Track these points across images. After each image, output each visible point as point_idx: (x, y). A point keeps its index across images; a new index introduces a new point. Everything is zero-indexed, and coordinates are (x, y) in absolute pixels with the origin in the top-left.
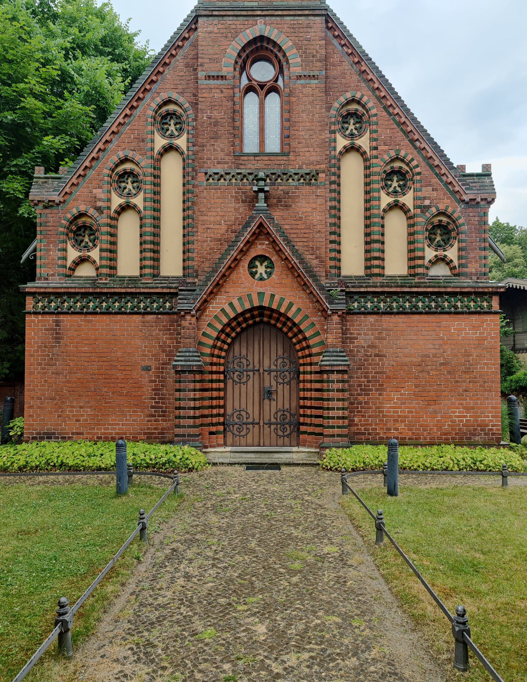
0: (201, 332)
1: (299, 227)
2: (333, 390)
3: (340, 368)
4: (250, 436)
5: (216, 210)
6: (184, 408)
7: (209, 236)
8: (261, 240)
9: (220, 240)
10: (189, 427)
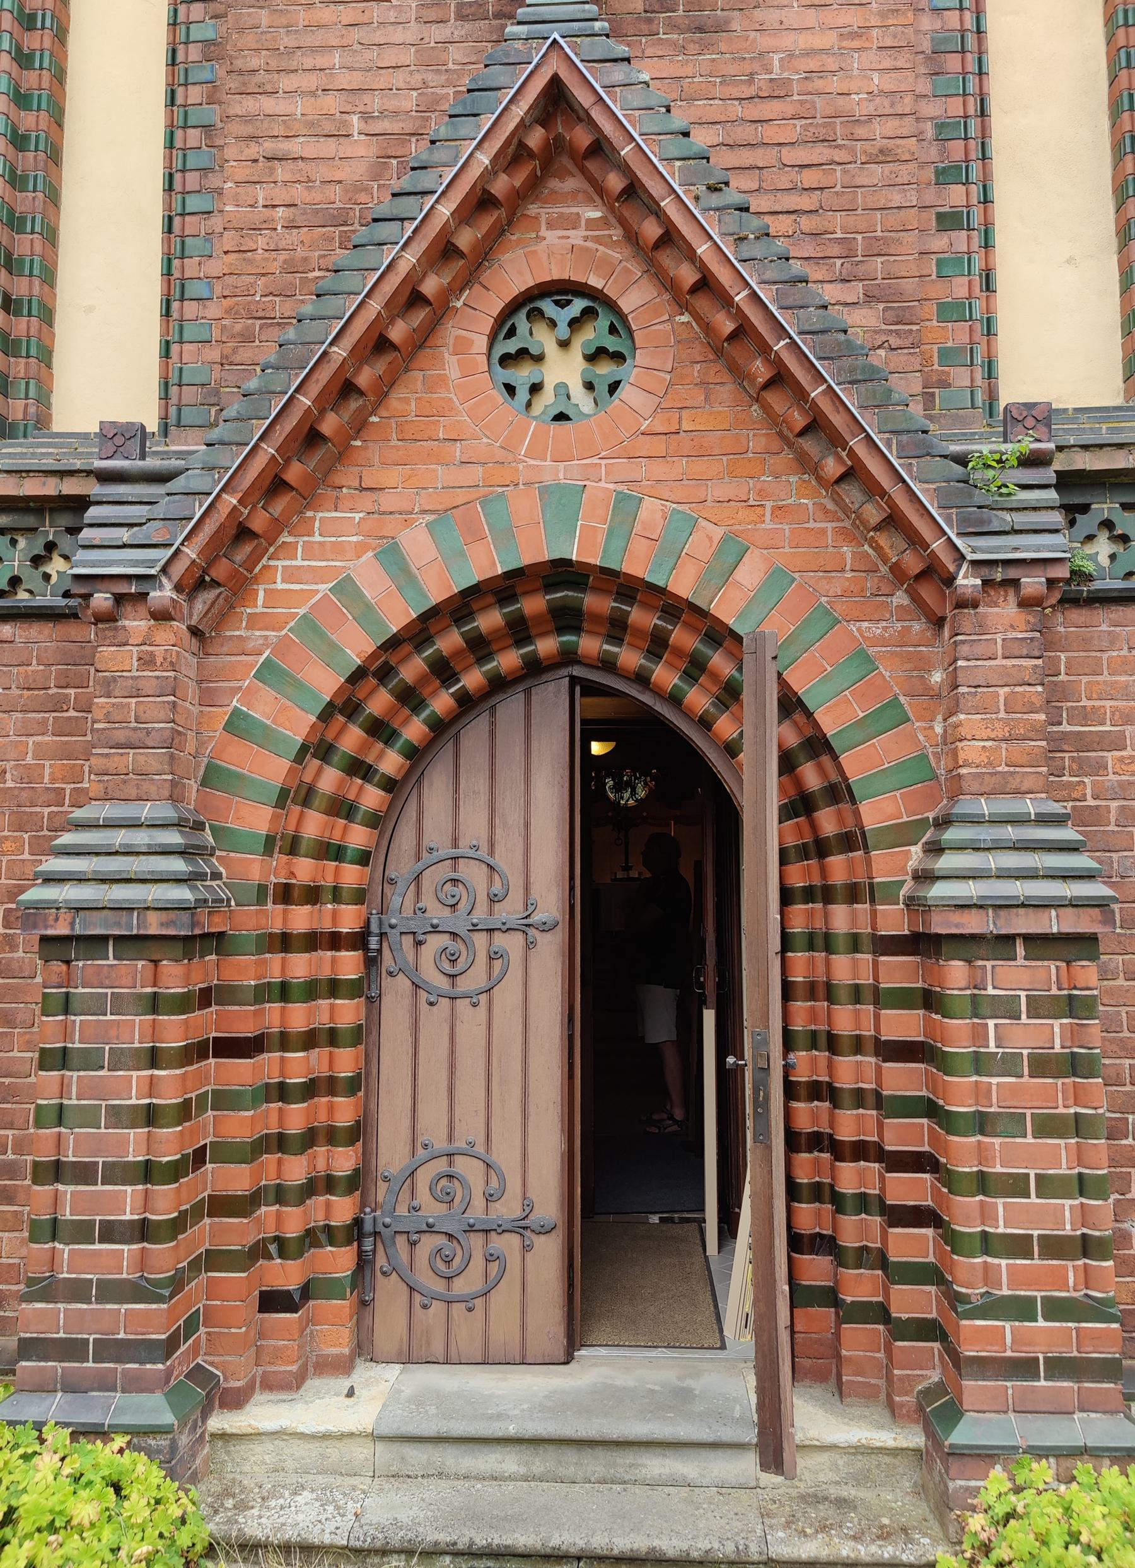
0: (222, 715)
1: (770, 133)
2: (1008, 1065)
3: (1053, 923)
4: (504, 1299)
5: (321, 61)
6: (84, 1173)
7: (281, 195)
8: (556, 198)
9: (340, 220)
10: (110, 1291)
